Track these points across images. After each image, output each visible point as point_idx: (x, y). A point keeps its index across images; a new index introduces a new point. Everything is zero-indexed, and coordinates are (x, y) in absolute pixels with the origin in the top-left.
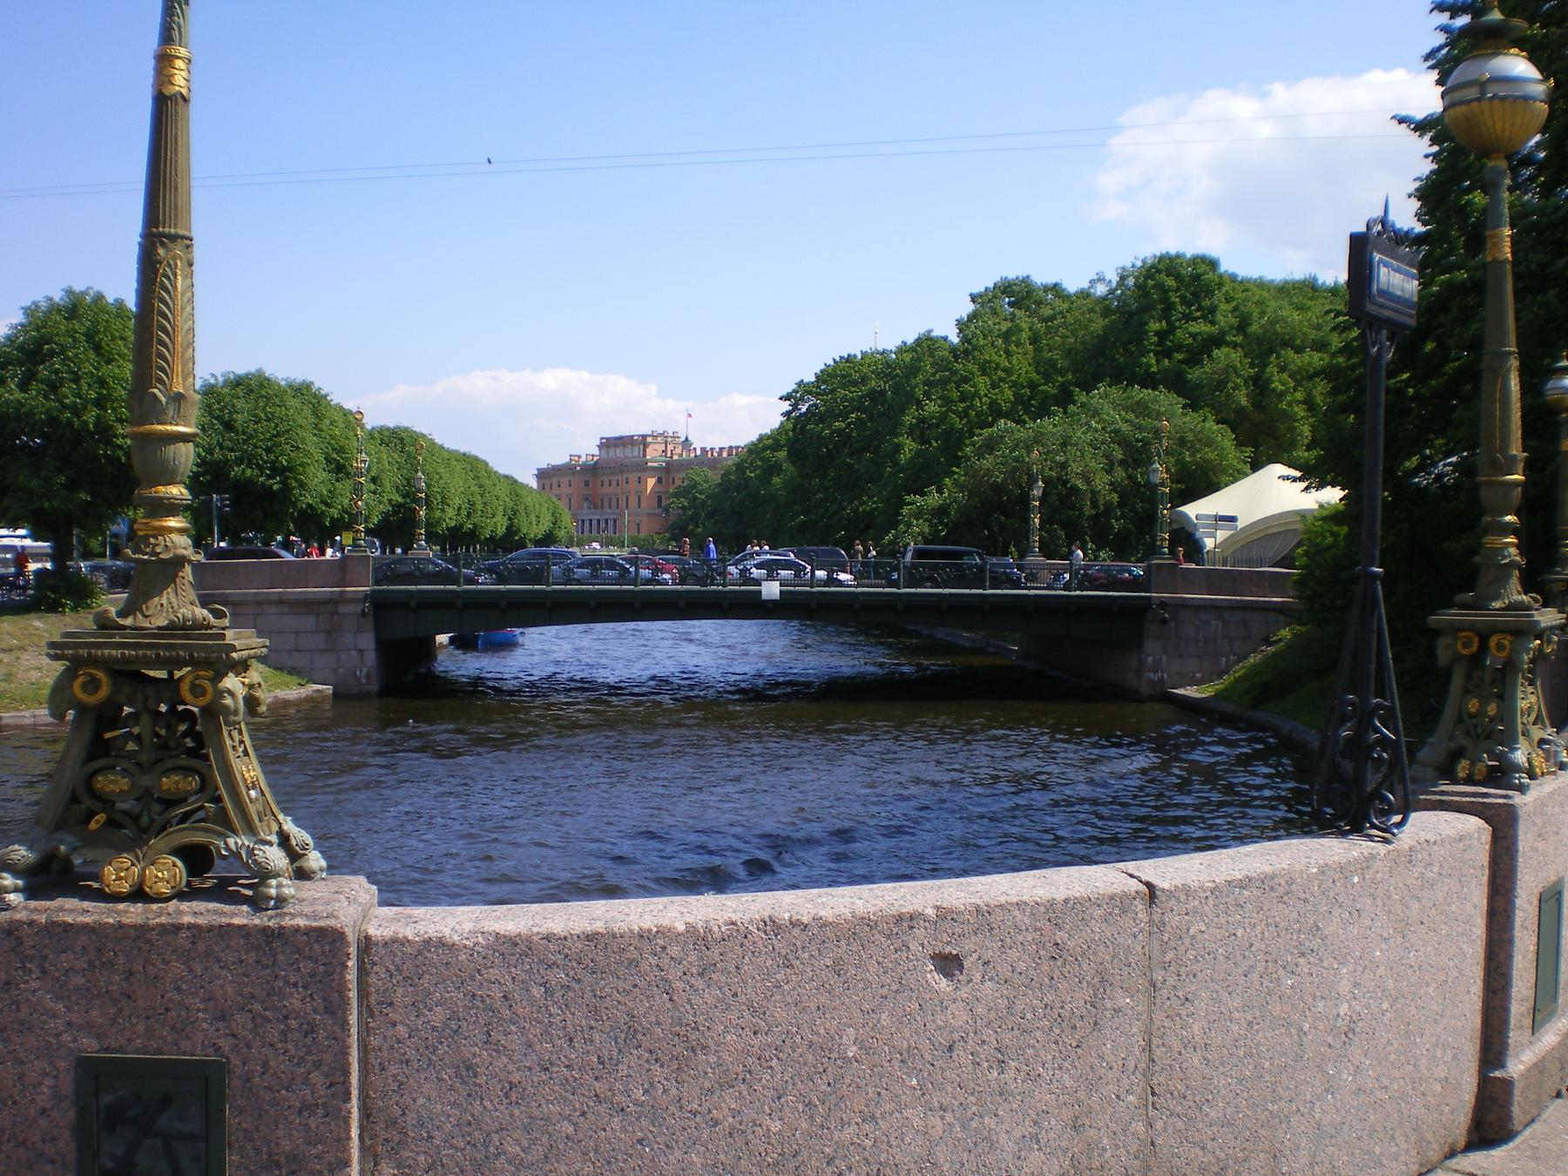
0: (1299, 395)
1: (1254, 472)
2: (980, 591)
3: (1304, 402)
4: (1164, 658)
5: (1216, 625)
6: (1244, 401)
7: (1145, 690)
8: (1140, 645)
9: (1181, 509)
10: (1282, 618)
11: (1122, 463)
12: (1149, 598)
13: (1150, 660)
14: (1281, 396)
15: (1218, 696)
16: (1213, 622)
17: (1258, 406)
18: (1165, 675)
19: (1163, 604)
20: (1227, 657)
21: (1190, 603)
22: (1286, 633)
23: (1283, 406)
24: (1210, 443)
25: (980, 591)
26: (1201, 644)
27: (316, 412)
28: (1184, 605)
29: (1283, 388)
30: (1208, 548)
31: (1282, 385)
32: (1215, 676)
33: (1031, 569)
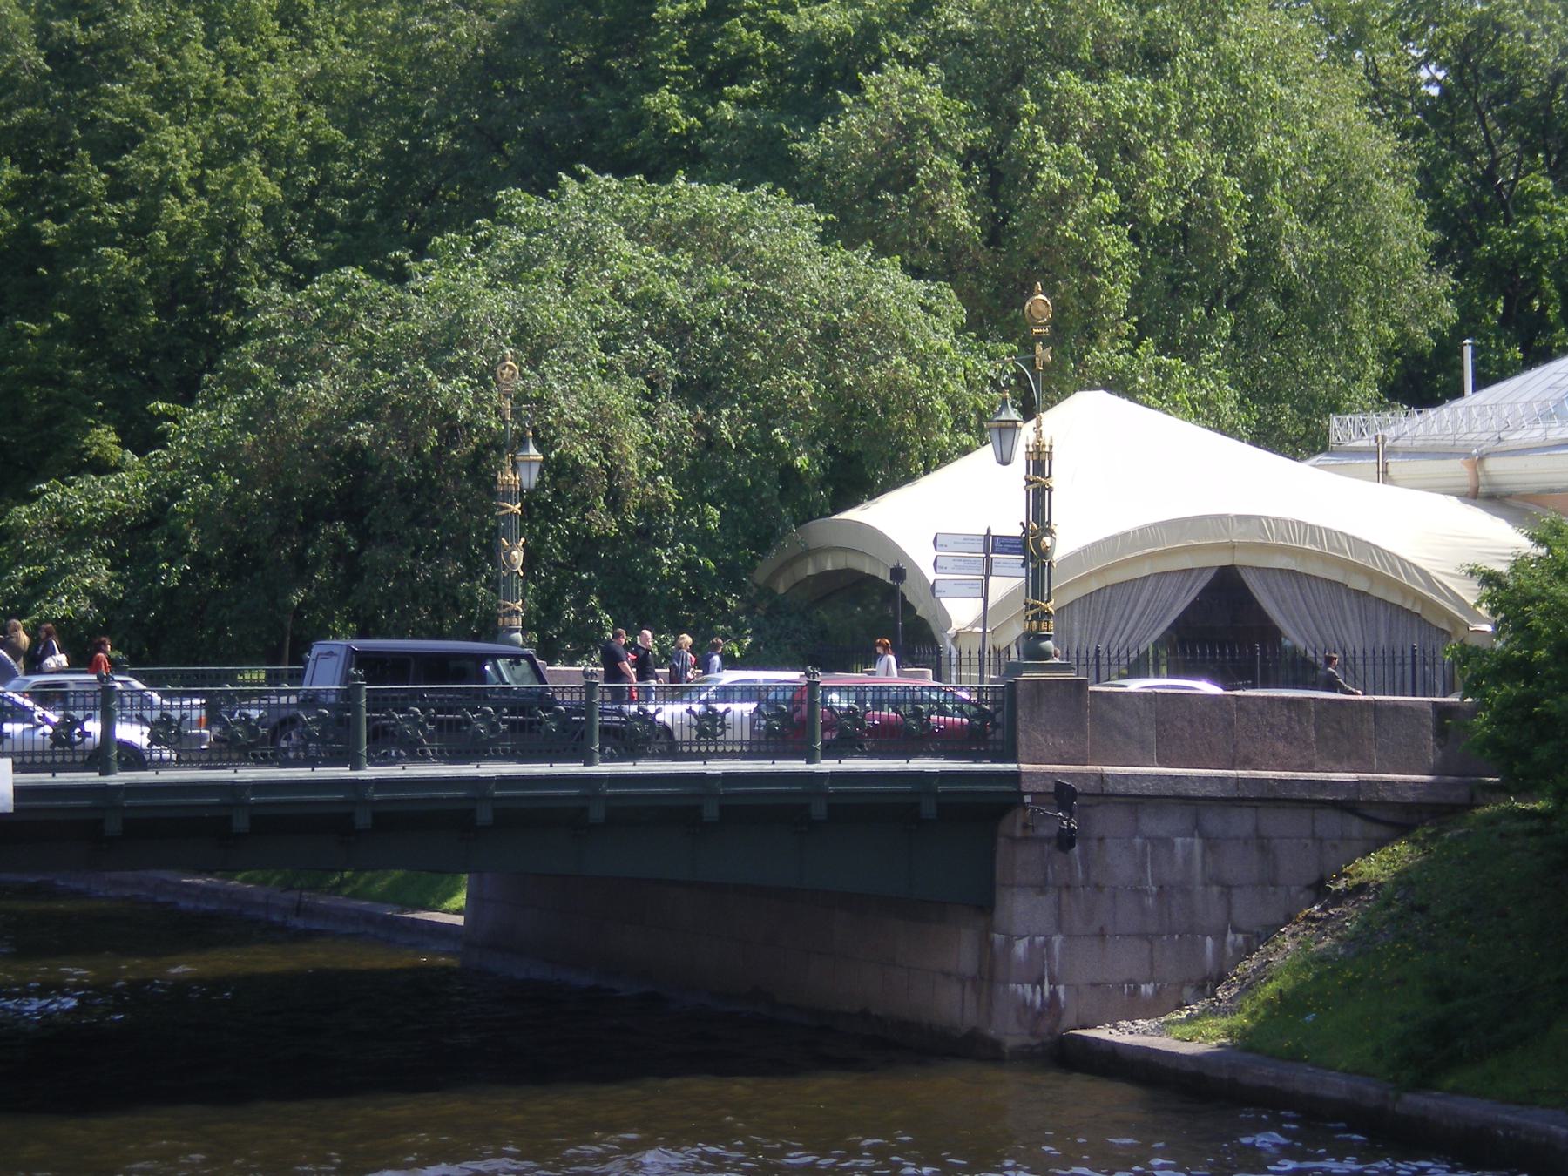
0: (1109, 201)
1: (1255, 442)
2: (799, 766)
3: (1119, 218)
4: (1057, 940)
5: (1186, 846)
6: (962, 218)
7: (1011, 1033)
8: (984, 905)
9: (853, 514)
10: (1355, 826)
11: (680, 388)
12: (1015, 776)
13: (1021, 947)
14: (1058, 202)
15: (1246, 1043)
16: (1178, 840)
17: (995, 235)
18: (1061, 989)
19: (1063, 794)
20: (1220, 936)
21: (1121, 789)
22: (1374, 867)
23: (1067, 230)
24: (890, 337)
25: (799, 766)
26: (1150, 901)
27: (1197, 415)
28: (1103, 795)
29: (1067, 182)
30: (955, 626)
31: (1066, 171)
32: (1188, 992)
33: (914, 701)
